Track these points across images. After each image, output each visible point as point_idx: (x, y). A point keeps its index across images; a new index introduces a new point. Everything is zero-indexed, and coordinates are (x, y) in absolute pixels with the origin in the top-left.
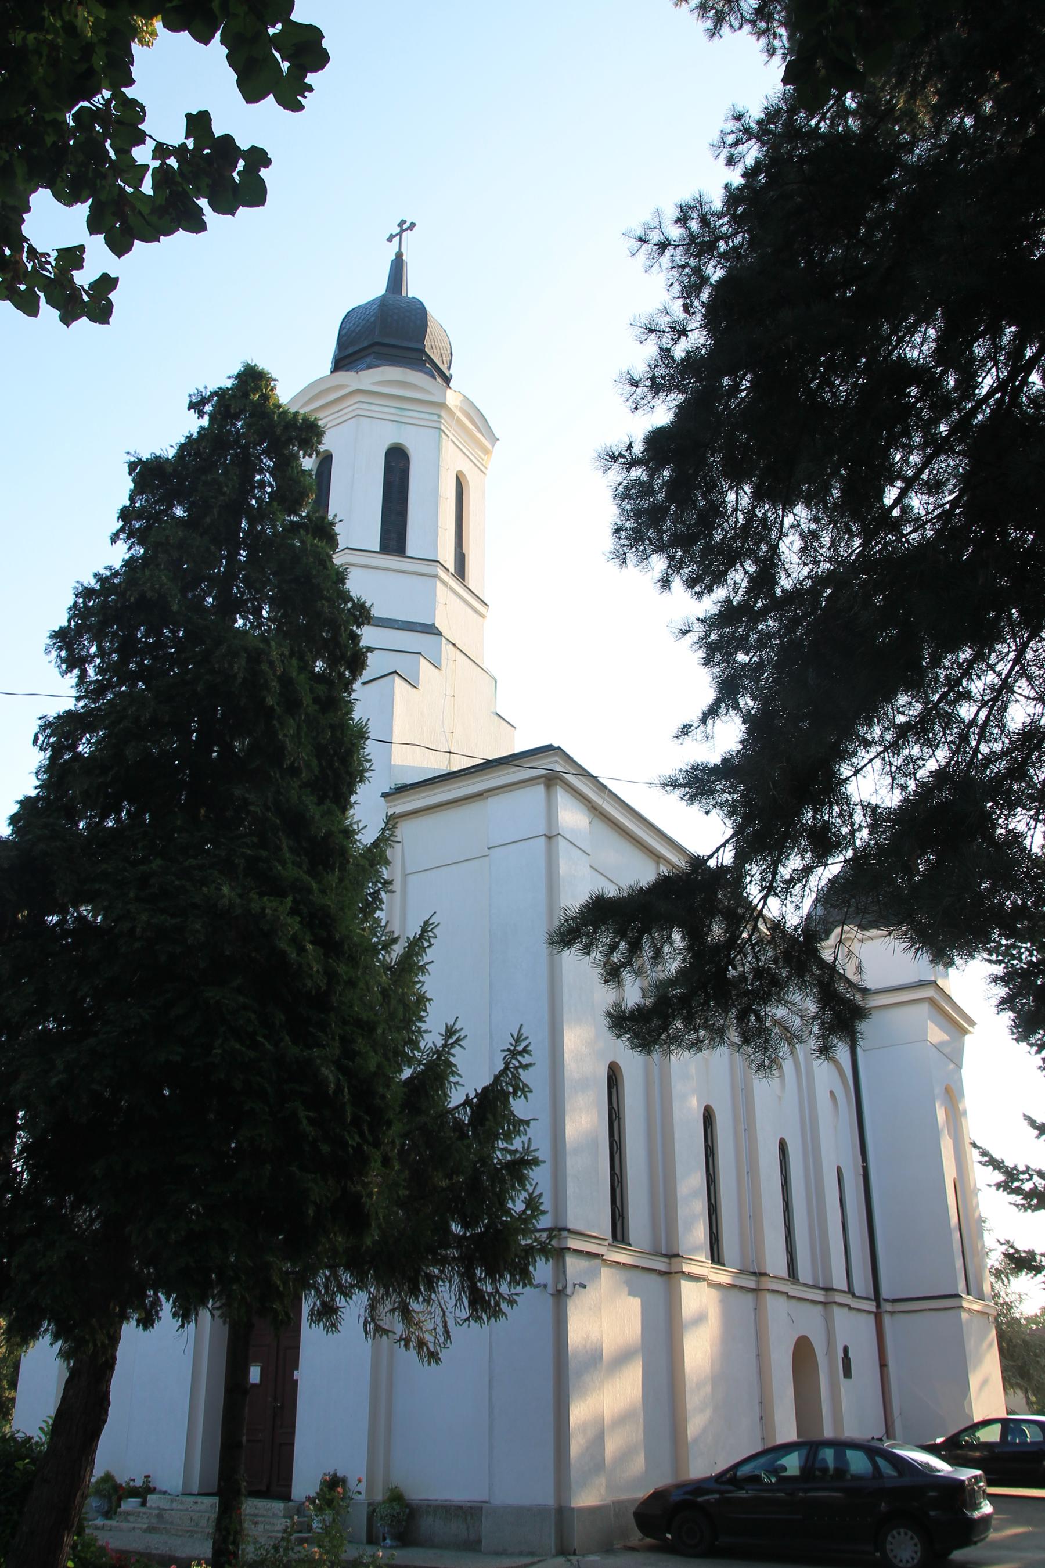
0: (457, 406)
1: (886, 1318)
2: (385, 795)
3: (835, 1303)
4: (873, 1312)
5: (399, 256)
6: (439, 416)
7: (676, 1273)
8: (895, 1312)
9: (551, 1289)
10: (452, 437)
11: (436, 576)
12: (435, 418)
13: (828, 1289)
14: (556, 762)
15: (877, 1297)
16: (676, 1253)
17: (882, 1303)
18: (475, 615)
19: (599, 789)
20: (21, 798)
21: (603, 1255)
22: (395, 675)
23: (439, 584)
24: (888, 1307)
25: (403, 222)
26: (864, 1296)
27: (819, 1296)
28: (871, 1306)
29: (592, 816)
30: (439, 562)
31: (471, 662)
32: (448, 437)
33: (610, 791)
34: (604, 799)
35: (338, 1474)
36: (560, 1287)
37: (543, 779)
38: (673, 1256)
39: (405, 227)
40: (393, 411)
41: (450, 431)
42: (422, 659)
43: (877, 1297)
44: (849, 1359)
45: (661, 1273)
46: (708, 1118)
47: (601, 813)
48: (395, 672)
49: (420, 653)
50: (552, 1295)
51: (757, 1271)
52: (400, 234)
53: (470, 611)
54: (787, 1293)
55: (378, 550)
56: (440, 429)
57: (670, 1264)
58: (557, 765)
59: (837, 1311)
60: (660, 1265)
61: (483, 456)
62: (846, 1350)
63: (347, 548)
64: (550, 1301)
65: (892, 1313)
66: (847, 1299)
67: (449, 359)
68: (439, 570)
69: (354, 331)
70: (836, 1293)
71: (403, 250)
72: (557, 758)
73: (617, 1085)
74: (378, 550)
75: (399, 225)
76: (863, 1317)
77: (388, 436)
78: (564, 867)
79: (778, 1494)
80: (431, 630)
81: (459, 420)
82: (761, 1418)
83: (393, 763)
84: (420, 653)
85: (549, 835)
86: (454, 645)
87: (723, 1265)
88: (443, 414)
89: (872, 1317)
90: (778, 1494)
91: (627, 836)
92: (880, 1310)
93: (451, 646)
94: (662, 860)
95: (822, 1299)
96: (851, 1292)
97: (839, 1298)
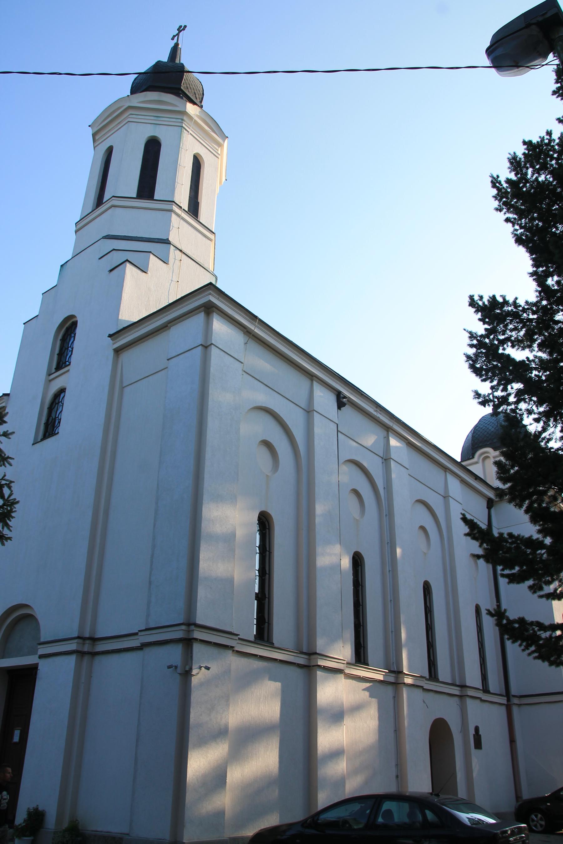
0: (197, 116)
1: (515, 709)
2: (110, 336)
3: (468, 696)
4: (504, 704)
5: (177, 45)
6: (182, 120)
7: (313, 666)
8: (521, 704)
9: (179, 670)
10: (191, 132)
11: (171, 211)
12: (180, 121)
13: (463, 686)
14: (210, 294)
15: (507, 693)
16: (314, 652)
17: (511, 697)
18: (204, 239)
19: (253, 320)
20: (518, 617)
21: (233, 647)
22: (127, 262)
23: (174, 216)
24: (516, 701)
25: (181, 27)
26: (499, 693)
27: (455, 691)
28: (504, 700)
29: (248, 338)
30: (174, 202)
31: (195, 263)
32: (188, 132)
33: (260, 320)
34: (256, 326)
35: (39, 809)
36: (187, 669)
37: (203, 308)
38: (312, 654)
39: (181, 29)
40: (152, 118)
41: (190, 129)
42: (151, 256)
43: (507, 693)
44: (480, 735)
45: (299, 666)
46: (427, 588)
47: (253, 335)
48: (127, 260)
49: (150, 252)
50: (180, 674)
51: (396, 670)
52: (178, 35)
53: (200, 235)
54: (422, 687)
55: (135, 196)
56: (182, 127)
57: (309, 659)
58: (210, 296)
59: (469, 701)
60: (301, 660)
61: (217, 148)
62: (477, 729)
63: (114, 196)
64: (178, 678)
65: (519, 705)
66: (480, 694)
67: (201, 97)
68: (174, 207)
69: (139, 83)
70: (468, 689)
71: (179, 42)
72: (211, 292)
73: (361, 566)
74: (135, 196)
75: (178, 30)
76: (494, 708)
77: (148, 132)
78: (318, 430)
79: (474, 826)
80: (167, 242)
81: (196, 123)
82: (397, 777)
83: (120, 318)
84: (150, 252)
85: (206, 345)
86: (181, 251)
87: (368, 665)
88: (185, 118)
89: (503, 709)
90: (474, 826)
91: (282, 358)
92: (509, 703)
93: (178, 251)
94: (314, 378)
95: (457, 693)
96: (486, 690)
97: (470, 693)
